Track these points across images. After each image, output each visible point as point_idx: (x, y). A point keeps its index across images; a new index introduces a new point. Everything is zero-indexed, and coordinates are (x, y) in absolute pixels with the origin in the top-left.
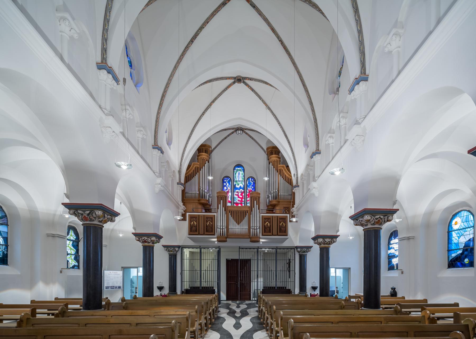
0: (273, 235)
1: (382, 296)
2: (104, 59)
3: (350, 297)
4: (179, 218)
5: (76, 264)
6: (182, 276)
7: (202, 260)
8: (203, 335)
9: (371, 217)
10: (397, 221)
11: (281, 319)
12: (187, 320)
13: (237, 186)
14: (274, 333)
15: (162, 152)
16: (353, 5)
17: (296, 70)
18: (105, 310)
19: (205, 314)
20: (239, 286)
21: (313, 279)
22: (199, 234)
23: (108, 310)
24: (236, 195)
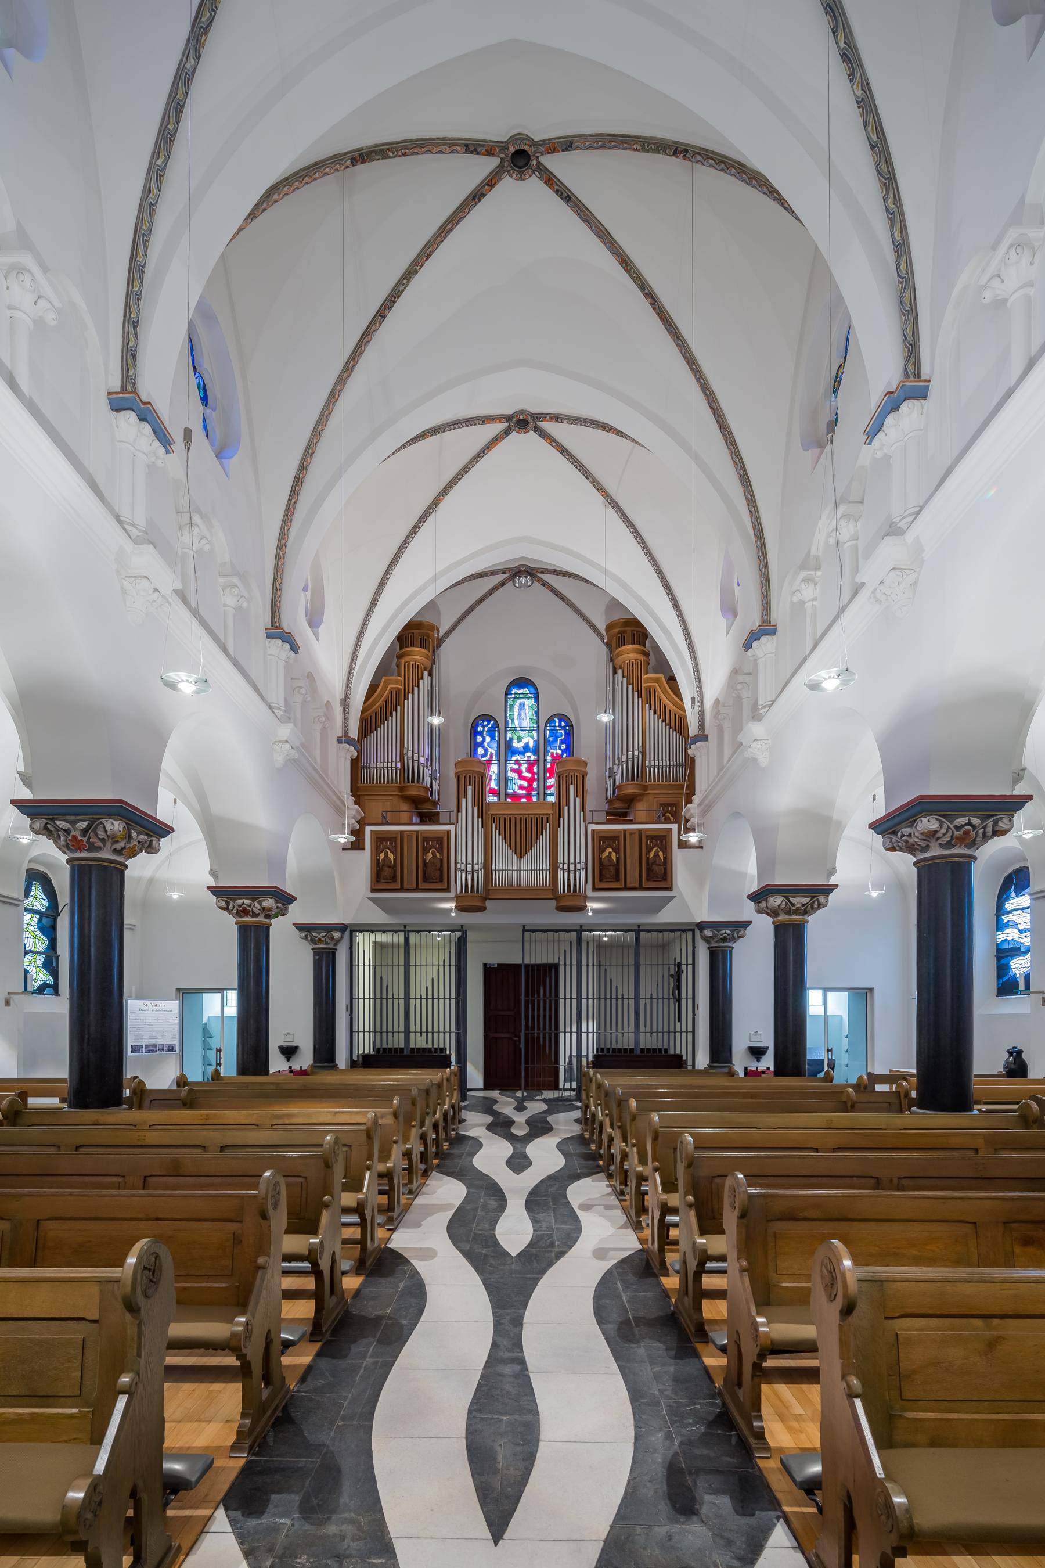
0: (626, 888)
1: (976, 1076)
2: (129, 380)
3: (874, 1079)
4: (343, 841)
5: (50, 980)
6: (351, 1014)
7: (412, 968)
8: (414, 1186)
9: (941, 824)
10: (1028, 836)
11: (655, 1138)
12: (369, 1136)
13: (516, 744)
14: (632, 1182)
15: (294, 648)
16: (877, 166)
17: (698, 380)
18: (131, 1108)
19: (422, 1124)
20: (522, 1046)
21: (753, 1022)
22: (402, 889)
23: (140, 1107)
24: (513, 770)
